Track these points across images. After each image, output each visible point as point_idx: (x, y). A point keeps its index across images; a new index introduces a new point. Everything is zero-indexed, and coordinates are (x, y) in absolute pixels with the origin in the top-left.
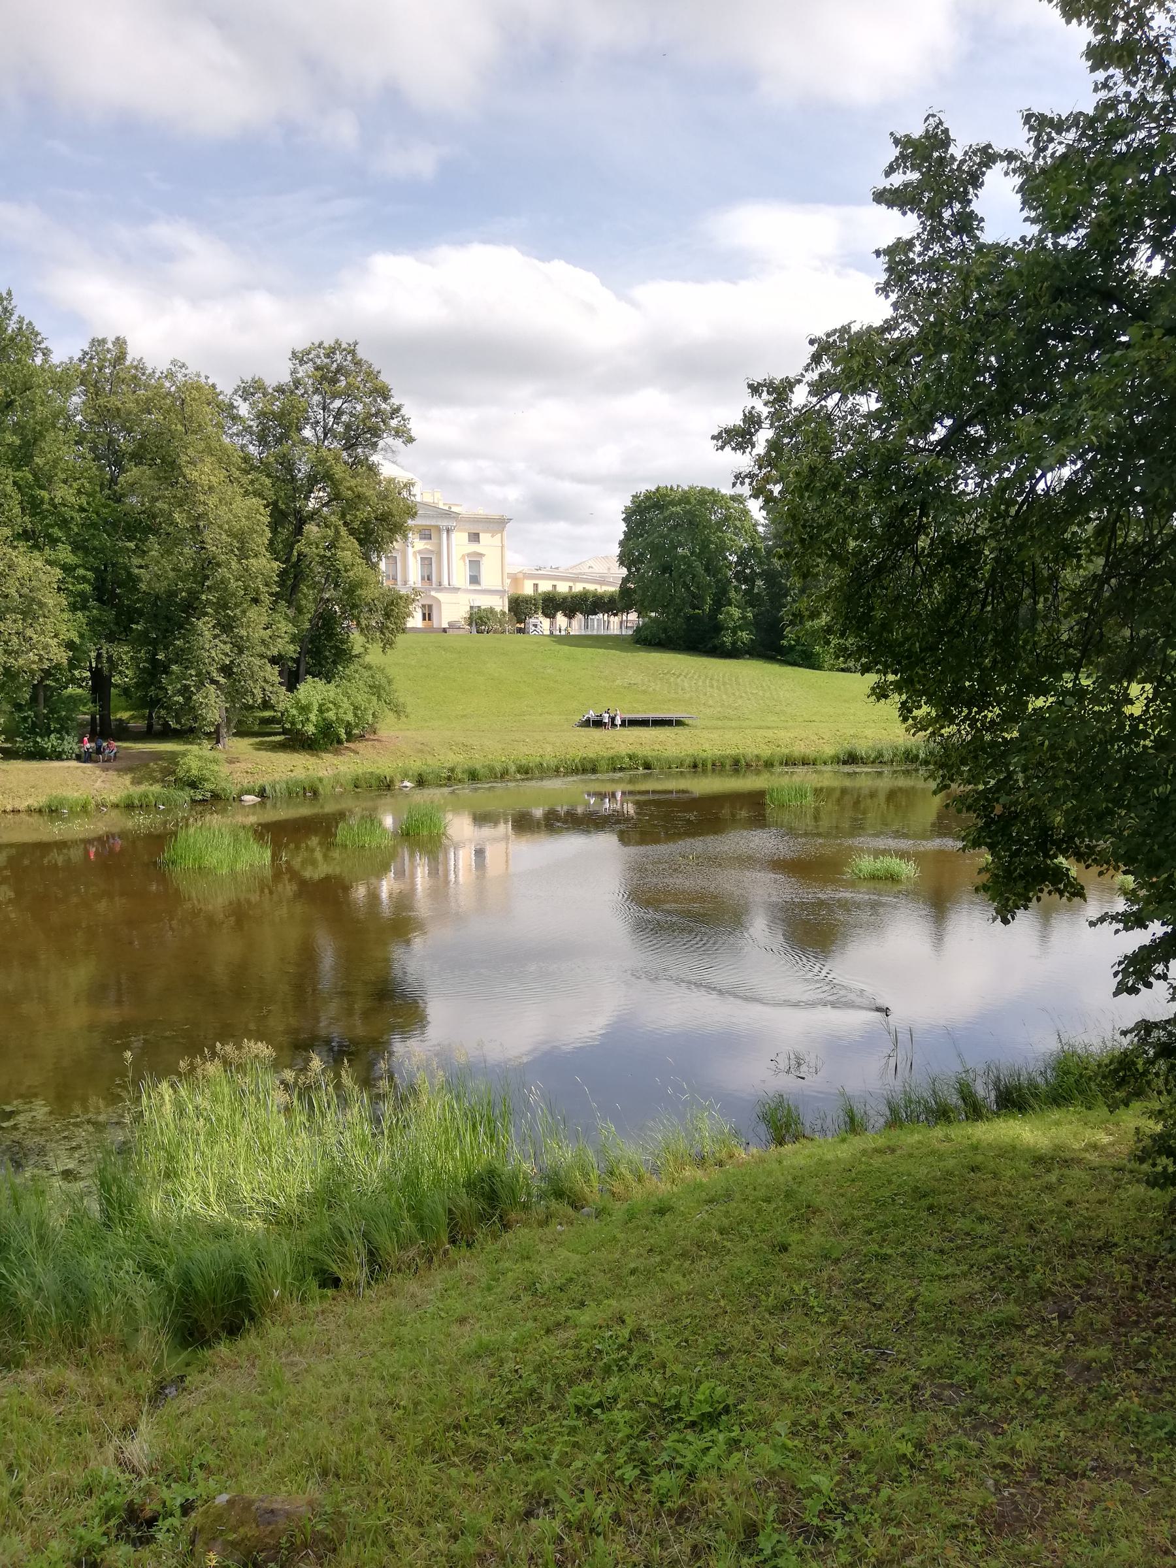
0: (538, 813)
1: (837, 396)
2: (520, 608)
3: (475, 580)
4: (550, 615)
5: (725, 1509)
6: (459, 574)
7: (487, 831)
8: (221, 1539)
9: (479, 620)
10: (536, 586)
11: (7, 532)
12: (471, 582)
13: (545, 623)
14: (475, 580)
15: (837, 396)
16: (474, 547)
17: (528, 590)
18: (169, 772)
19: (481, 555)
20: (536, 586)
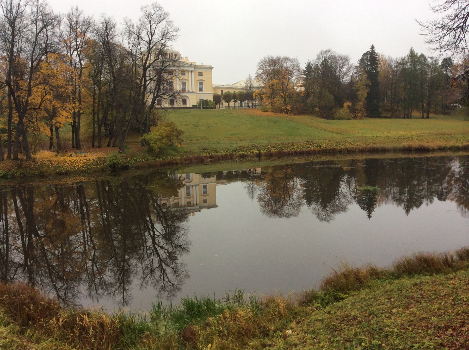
0: (225, 172)
1: (210, 345)
2: (217, 99)
3: (201, 90)
4: (228, 102)
5: (430, 283)
6: (196, 88)
7: (207, 180)
8: (37, 87)
9: (204, 104)
10: (222, 91)
11: (22, 4)
12: (200, 91)
13: (226, 104)
14: (201, 90)
15: (210, 345)
16: (201, 78)
17: (219, 93)
18: (132, 324)
19: (203, 80)
20: (222, 91)
